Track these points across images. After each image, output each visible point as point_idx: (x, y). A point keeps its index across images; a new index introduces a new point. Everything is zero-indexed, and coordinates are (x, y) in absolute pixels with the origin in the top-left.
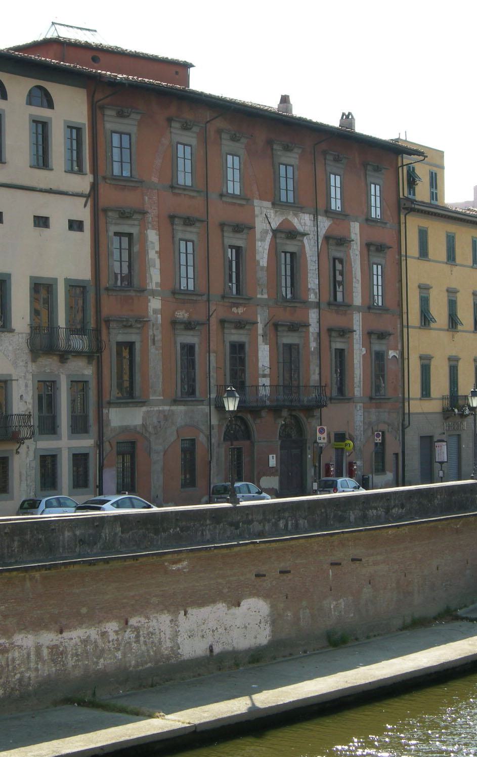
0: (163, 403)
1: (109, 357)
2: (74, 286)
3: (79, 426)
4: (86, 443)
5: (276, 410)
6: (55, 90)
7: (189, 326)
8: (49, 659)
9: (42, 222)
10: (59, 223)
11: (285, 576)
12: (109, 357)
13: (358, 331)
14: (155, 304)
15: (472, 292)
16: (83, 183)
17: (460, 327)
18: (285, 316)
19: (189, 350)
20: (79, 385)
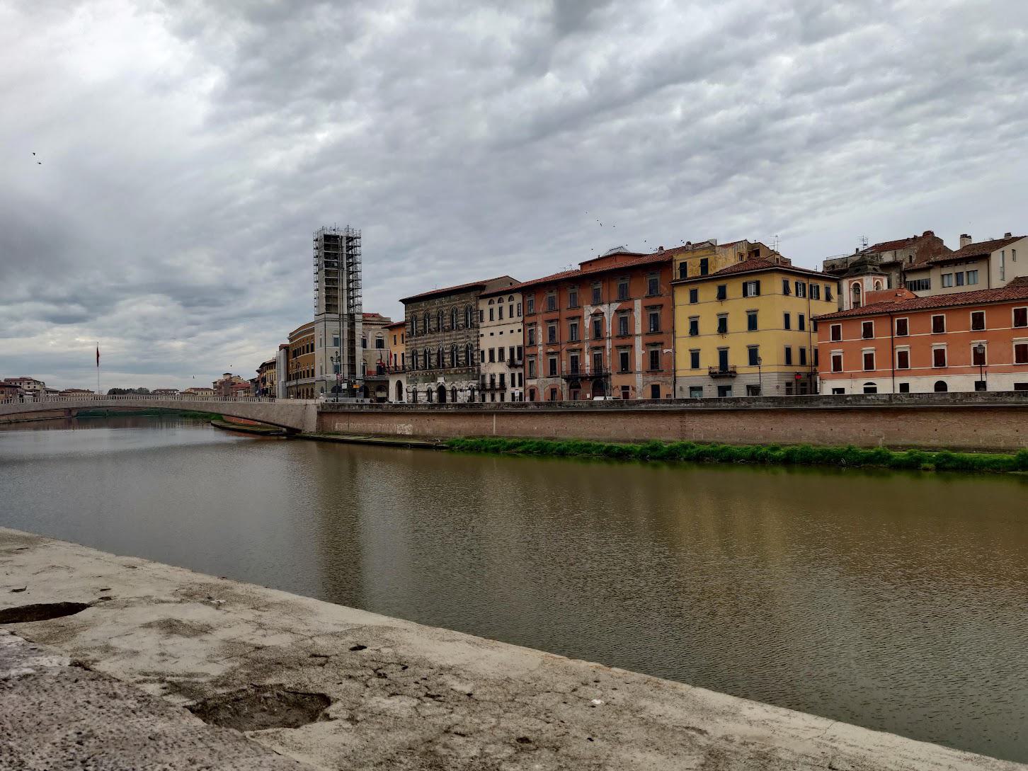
0: (544, 378)
1: (527, 365)
2: (519, 348)
3: (520, 385)
4: (522, 389)
5: (591, 378)
6: (513, 295)
7: (553, 354)
8: (10, 675)
9: (492, 334)
10: (516, 331)
11: (761, 323)
12: (527, 365)
13: (430, 386)
14: (541, 348)
15: (176, 40)
16: (521, 319)
17: (832, 300)
18: (596, 344)
19: (553, 362)
20: (520, 375)
